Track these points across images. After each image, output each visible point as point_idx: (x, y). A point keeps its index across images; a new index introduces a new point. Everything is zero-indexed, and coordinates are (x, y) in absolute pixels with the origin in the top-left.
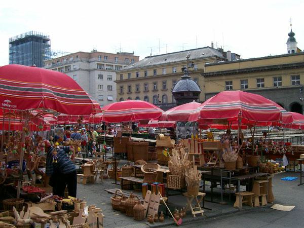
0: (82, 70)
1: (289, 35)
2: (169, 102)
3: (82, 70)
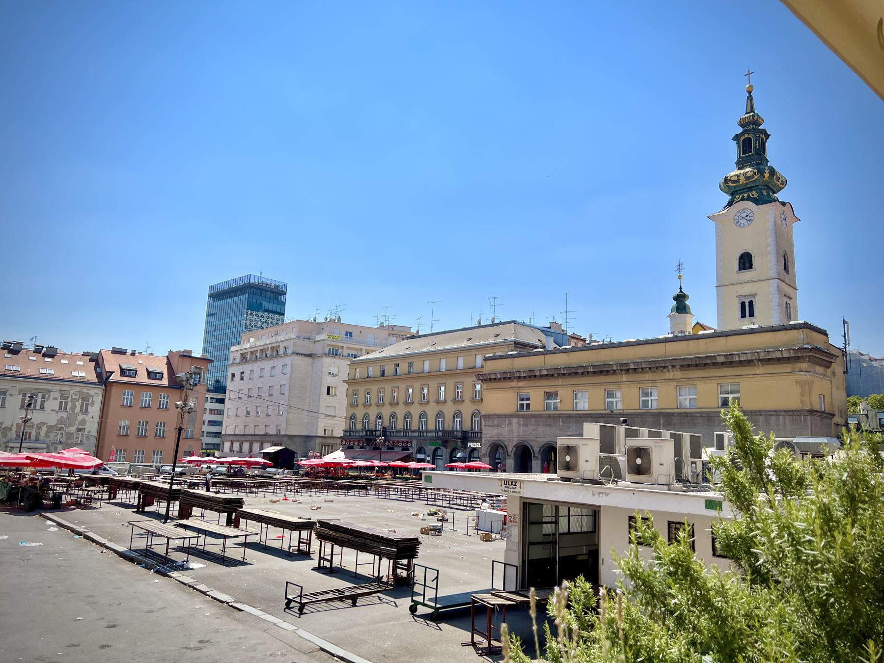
0: (297, 354)
1: (675, 299)
2: (446, 429)
3: (297, 354)
